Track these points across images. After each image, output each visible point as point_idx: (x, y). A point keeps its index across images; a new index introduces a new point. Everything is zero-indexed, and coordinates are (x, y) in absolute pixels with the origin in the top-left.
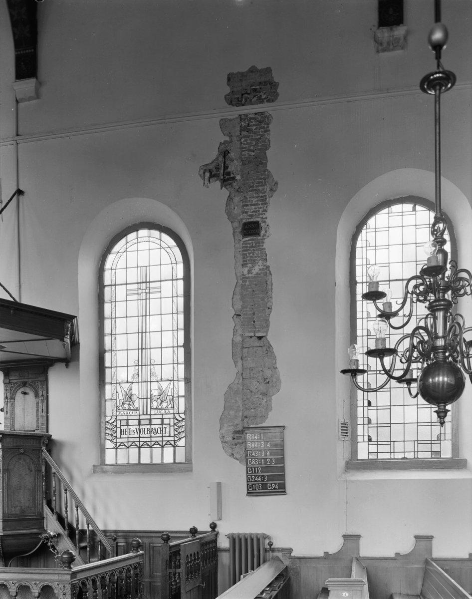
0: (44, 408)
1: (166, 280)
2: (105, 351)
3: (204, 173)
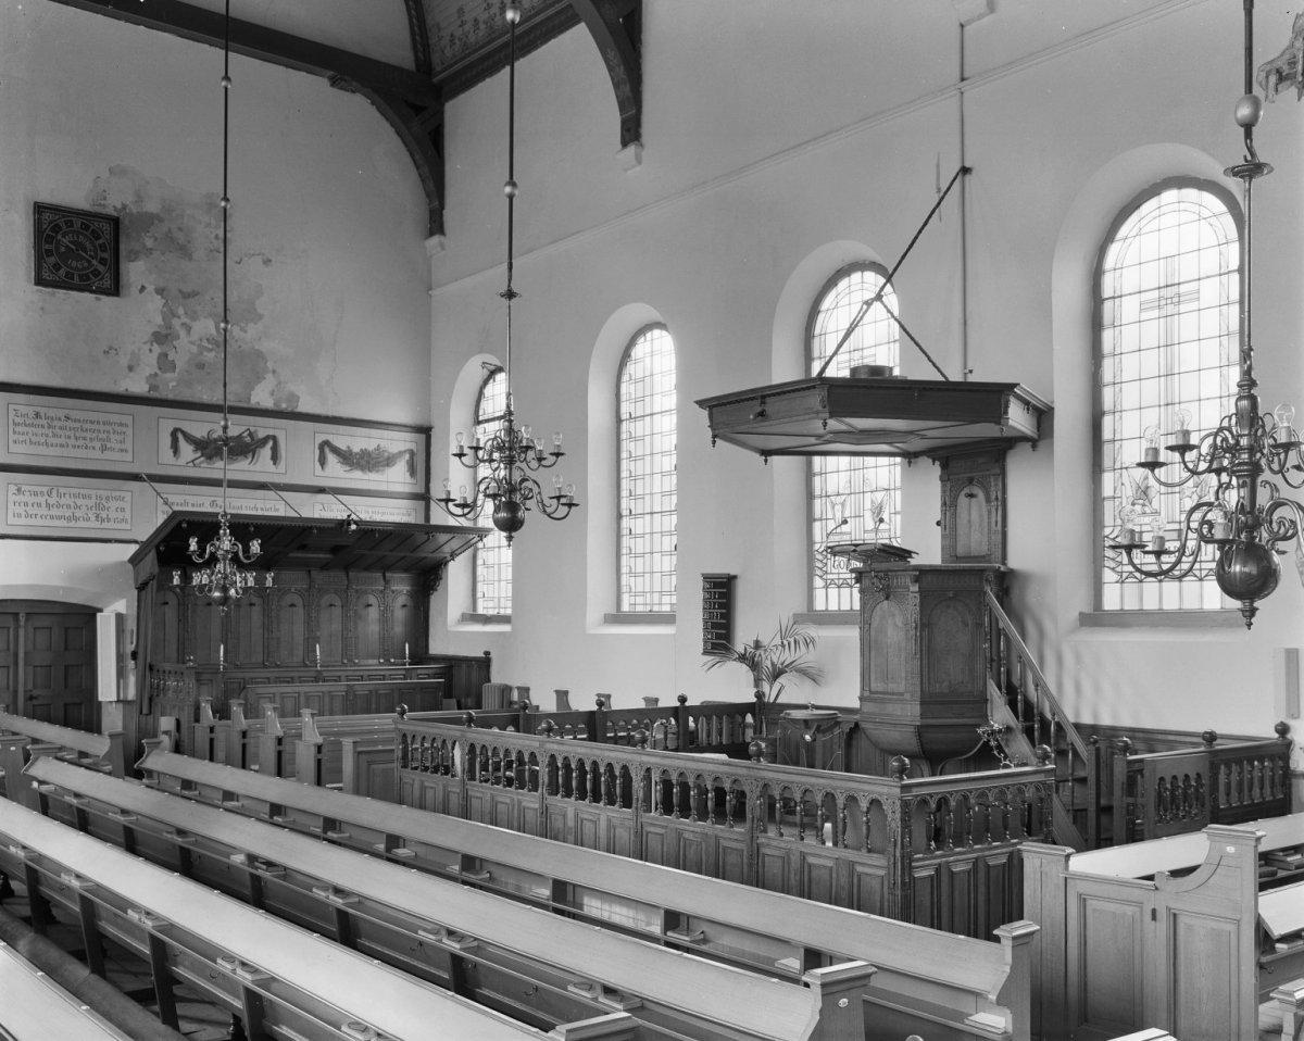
0: (999, 519)
1: (1208, 277)
2: (1102, 414)
3: (1267, 77)
